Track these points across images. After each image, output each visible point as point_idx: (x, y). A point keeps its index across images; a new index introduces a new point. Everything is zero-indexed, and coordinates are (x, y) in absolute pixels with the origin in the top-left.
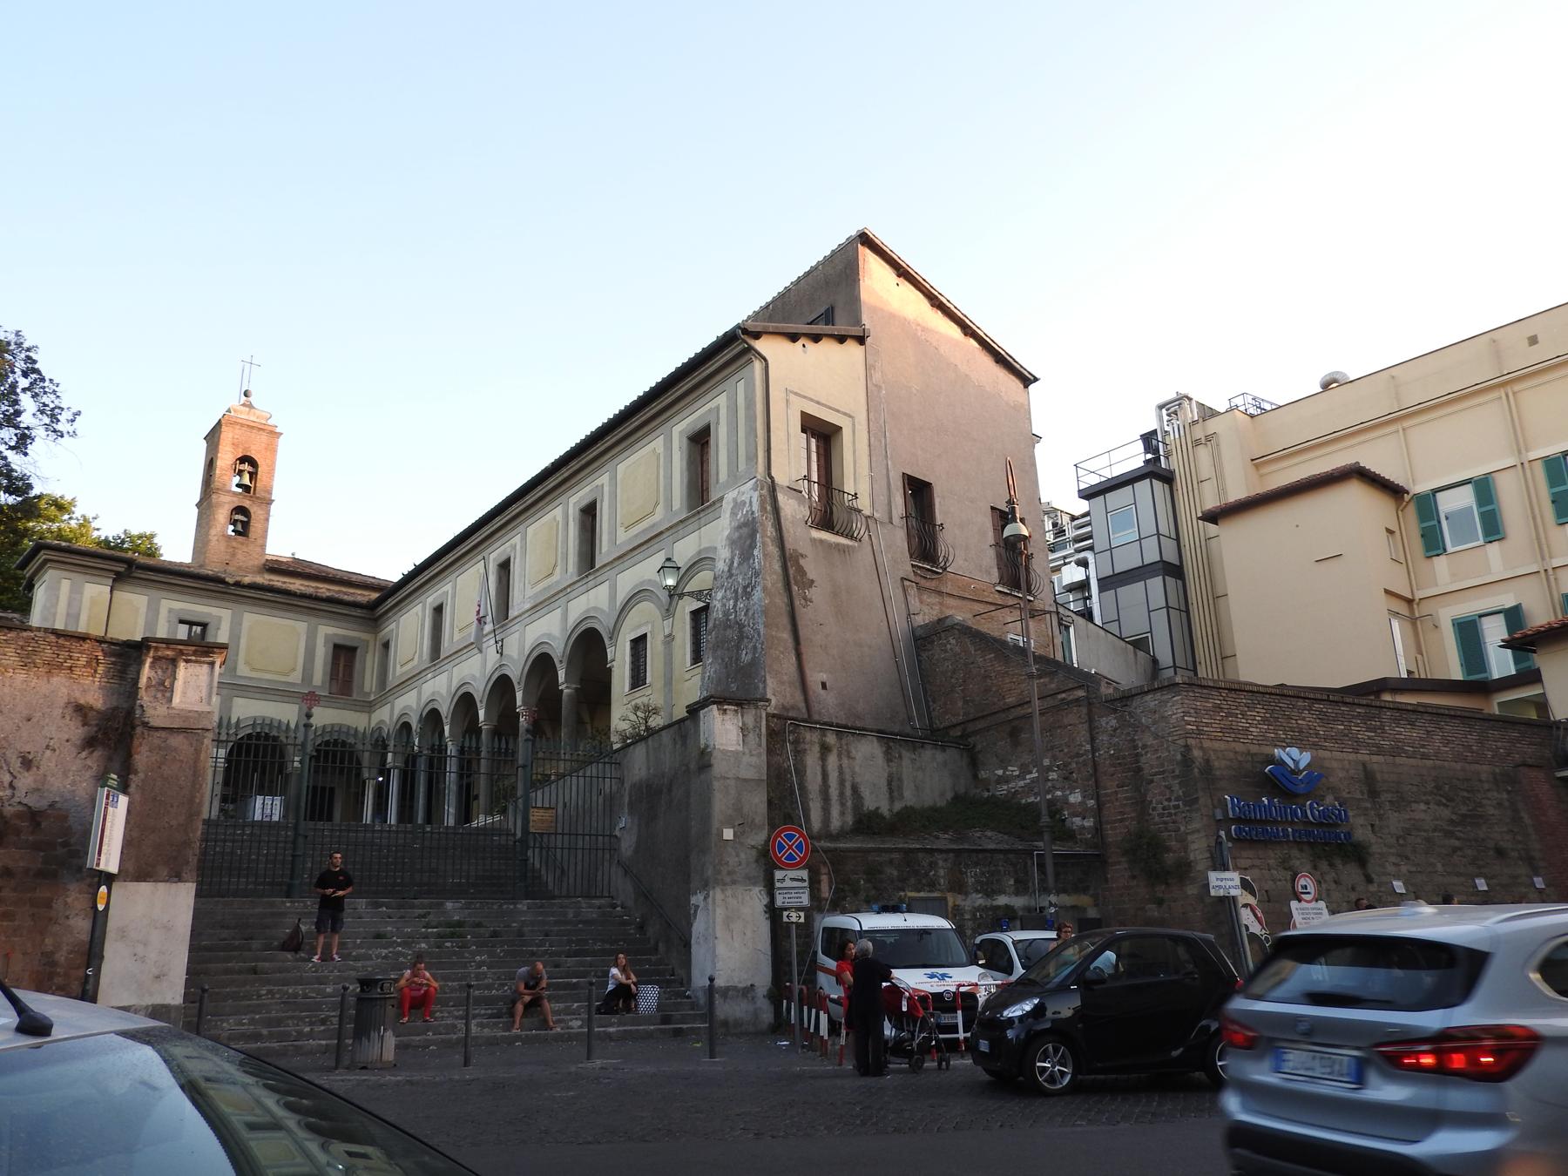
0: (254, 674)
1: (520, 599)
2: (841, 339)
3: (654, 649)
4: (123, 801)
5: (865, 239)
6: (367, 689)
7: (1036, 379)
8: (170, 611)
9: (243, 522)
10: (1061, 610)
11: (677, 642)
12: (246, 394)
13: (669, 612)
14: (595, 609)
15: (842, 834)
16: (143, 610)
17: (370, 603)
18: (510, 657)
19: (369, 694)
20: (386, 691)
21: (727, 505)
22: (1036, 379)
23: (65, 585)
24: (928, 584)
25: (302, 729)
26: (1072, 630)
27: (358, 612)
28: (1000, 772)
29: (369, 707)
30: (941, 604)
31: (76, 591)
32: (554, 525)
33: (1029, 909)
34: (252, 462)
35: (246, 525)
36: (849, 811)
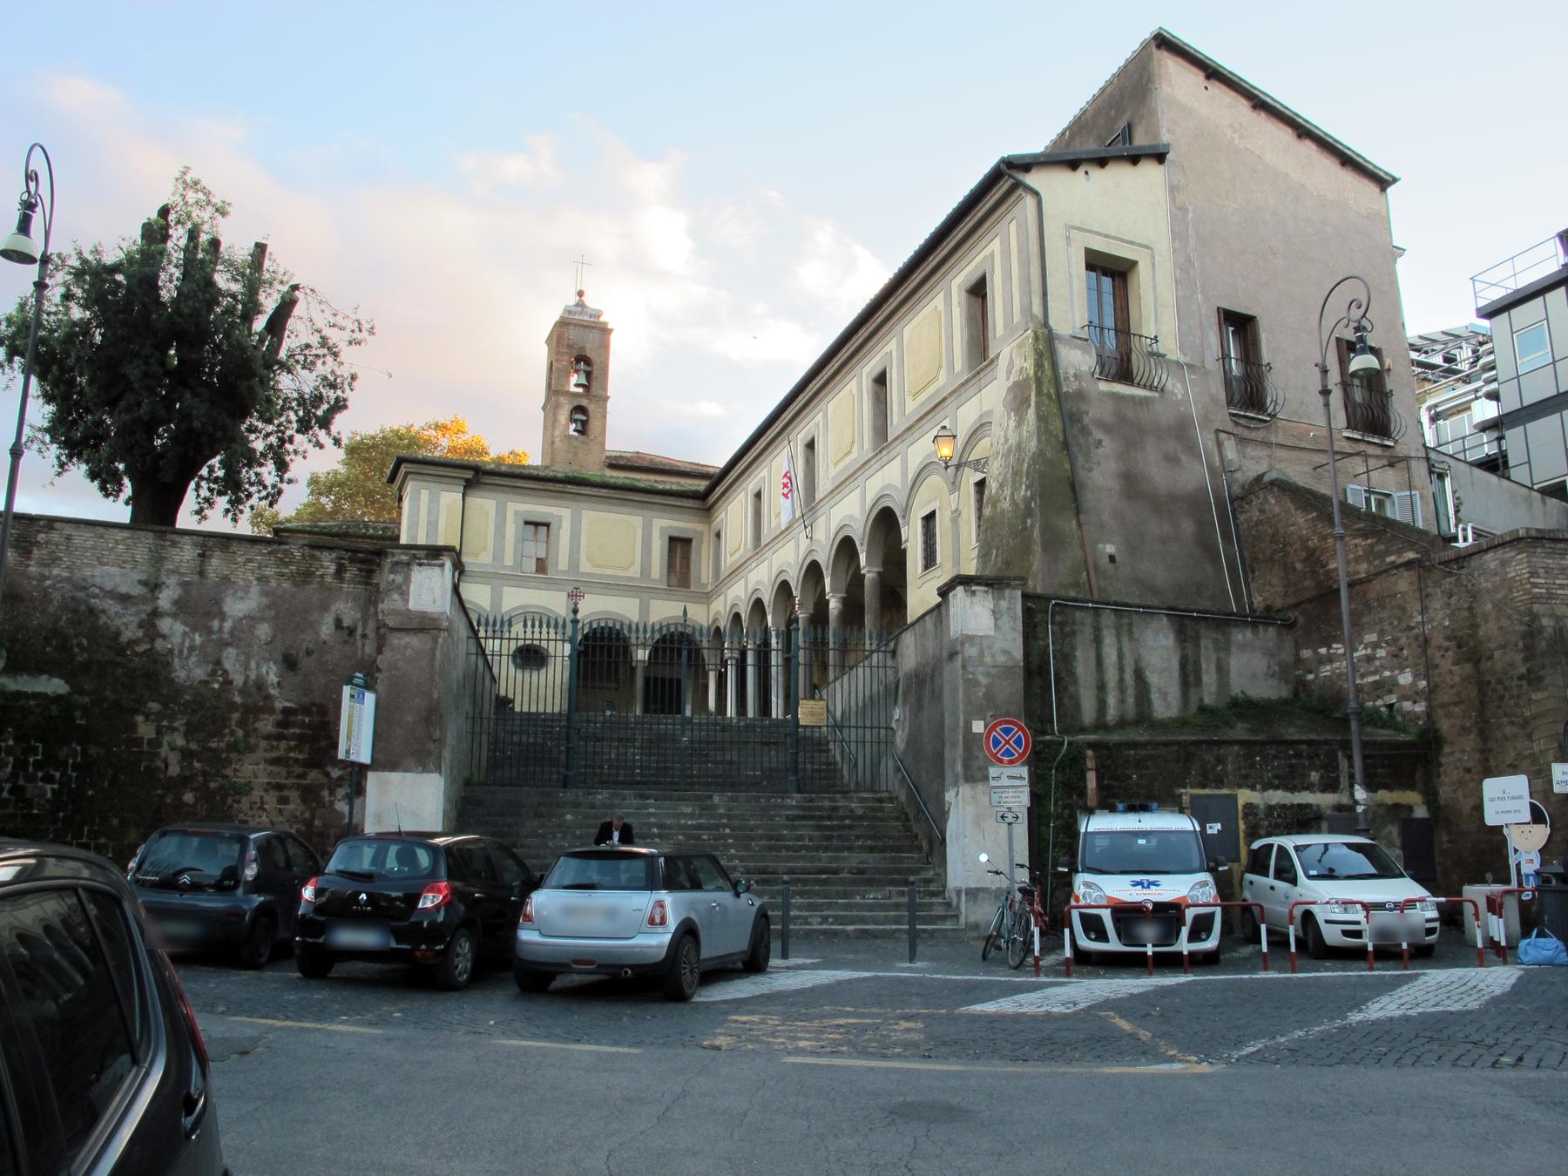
1: (826, 479)
2: (1134, 160)
3: (942, 526)
4: (370, 698)
5: (1163, 42)
6: (704, 580)
7: (1395, 180)
8: (516, 513)
9: (584, 417)
10: (1433, 455)
11: (964, 516)
12: (581, 294)
13: (954, 485)
14: (889, 486)
15: (1122, 724)
16: (493, 514)
17: (702, 491)
18: (819, 541)
19: (706, 586)
20: (722, 581)
21: (1003, 363)
22: (1395, 180)
23: (425, 494)
24: (1253, 435)
25: (569, 626)
26: (1448, 481)
28: (1323, 651)
29: (706, 597)
30: (1270, 456)
31: (434, 500)
32: (848, 401)
33: (1339, 808)
34: (588, 362)
35: (584, 423)
36: (1131, 700)
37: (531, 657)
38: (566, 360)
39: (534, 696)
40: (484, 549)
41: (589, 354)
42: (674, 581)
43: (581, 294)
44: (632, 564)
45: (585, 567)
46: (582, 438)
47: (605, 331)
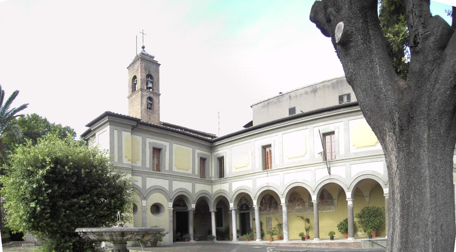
8: (150, 143)
12: (143, 48)
28: (94, 216)
29: (211, 183)
35: (151, 104)
37: (157, 208)
40: (189, 168)
41: (153, 74)
43: (143, 48)
45: (175, 169)
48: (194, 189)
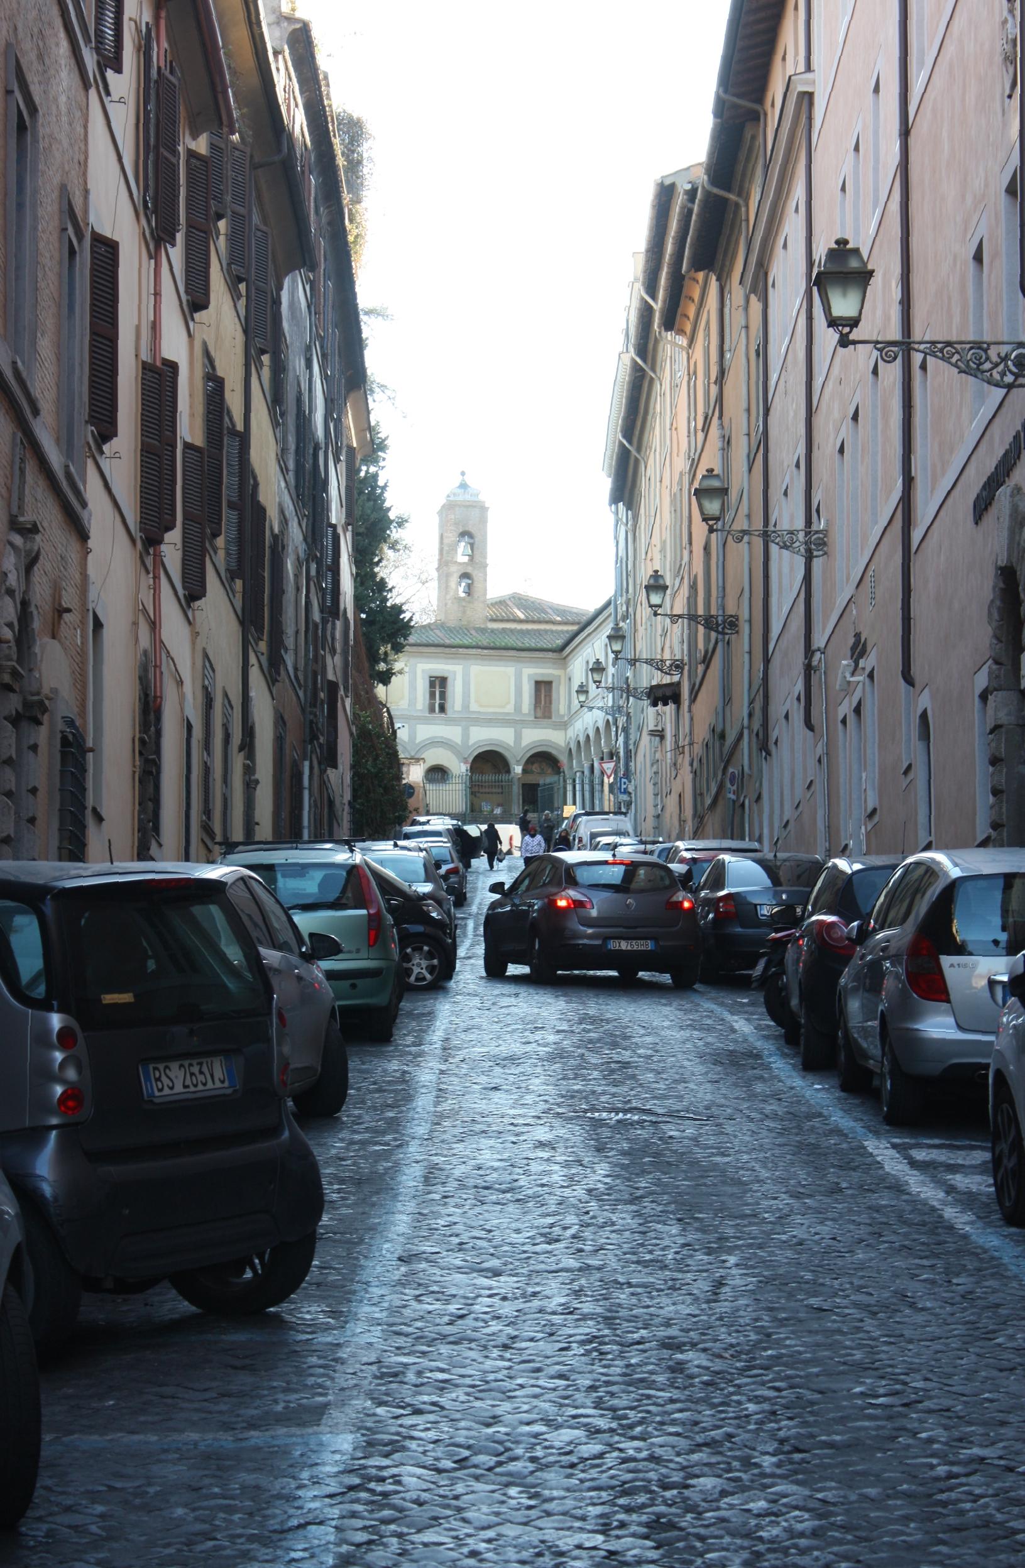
0: (482, 710)
8: (423, 671)
12: (463, 474)
19: (563, 716)
27: (550, 655)
29: (564, 726)
38: (451, 537)
39: (777, 799)
41: (470, 528)
42: (539, 714)
43: (463, 474)
44: (508, 703)
45: (474, 707)
46: (468, 599)
47: (483, 509)
48: (518, 740)
